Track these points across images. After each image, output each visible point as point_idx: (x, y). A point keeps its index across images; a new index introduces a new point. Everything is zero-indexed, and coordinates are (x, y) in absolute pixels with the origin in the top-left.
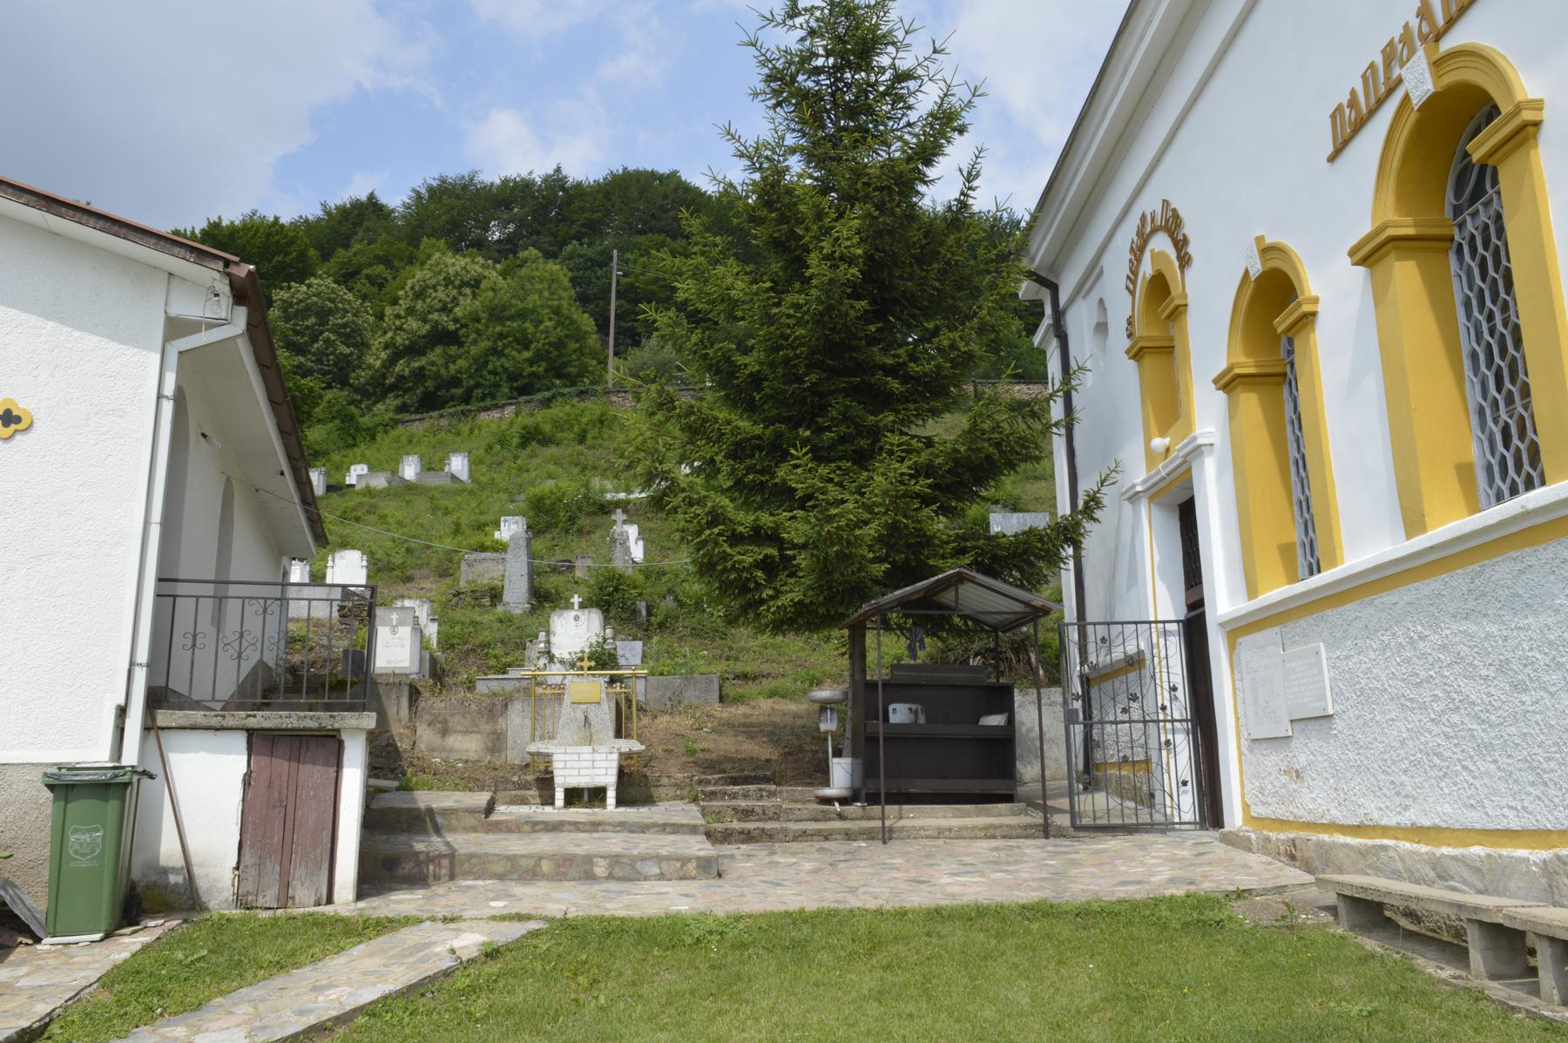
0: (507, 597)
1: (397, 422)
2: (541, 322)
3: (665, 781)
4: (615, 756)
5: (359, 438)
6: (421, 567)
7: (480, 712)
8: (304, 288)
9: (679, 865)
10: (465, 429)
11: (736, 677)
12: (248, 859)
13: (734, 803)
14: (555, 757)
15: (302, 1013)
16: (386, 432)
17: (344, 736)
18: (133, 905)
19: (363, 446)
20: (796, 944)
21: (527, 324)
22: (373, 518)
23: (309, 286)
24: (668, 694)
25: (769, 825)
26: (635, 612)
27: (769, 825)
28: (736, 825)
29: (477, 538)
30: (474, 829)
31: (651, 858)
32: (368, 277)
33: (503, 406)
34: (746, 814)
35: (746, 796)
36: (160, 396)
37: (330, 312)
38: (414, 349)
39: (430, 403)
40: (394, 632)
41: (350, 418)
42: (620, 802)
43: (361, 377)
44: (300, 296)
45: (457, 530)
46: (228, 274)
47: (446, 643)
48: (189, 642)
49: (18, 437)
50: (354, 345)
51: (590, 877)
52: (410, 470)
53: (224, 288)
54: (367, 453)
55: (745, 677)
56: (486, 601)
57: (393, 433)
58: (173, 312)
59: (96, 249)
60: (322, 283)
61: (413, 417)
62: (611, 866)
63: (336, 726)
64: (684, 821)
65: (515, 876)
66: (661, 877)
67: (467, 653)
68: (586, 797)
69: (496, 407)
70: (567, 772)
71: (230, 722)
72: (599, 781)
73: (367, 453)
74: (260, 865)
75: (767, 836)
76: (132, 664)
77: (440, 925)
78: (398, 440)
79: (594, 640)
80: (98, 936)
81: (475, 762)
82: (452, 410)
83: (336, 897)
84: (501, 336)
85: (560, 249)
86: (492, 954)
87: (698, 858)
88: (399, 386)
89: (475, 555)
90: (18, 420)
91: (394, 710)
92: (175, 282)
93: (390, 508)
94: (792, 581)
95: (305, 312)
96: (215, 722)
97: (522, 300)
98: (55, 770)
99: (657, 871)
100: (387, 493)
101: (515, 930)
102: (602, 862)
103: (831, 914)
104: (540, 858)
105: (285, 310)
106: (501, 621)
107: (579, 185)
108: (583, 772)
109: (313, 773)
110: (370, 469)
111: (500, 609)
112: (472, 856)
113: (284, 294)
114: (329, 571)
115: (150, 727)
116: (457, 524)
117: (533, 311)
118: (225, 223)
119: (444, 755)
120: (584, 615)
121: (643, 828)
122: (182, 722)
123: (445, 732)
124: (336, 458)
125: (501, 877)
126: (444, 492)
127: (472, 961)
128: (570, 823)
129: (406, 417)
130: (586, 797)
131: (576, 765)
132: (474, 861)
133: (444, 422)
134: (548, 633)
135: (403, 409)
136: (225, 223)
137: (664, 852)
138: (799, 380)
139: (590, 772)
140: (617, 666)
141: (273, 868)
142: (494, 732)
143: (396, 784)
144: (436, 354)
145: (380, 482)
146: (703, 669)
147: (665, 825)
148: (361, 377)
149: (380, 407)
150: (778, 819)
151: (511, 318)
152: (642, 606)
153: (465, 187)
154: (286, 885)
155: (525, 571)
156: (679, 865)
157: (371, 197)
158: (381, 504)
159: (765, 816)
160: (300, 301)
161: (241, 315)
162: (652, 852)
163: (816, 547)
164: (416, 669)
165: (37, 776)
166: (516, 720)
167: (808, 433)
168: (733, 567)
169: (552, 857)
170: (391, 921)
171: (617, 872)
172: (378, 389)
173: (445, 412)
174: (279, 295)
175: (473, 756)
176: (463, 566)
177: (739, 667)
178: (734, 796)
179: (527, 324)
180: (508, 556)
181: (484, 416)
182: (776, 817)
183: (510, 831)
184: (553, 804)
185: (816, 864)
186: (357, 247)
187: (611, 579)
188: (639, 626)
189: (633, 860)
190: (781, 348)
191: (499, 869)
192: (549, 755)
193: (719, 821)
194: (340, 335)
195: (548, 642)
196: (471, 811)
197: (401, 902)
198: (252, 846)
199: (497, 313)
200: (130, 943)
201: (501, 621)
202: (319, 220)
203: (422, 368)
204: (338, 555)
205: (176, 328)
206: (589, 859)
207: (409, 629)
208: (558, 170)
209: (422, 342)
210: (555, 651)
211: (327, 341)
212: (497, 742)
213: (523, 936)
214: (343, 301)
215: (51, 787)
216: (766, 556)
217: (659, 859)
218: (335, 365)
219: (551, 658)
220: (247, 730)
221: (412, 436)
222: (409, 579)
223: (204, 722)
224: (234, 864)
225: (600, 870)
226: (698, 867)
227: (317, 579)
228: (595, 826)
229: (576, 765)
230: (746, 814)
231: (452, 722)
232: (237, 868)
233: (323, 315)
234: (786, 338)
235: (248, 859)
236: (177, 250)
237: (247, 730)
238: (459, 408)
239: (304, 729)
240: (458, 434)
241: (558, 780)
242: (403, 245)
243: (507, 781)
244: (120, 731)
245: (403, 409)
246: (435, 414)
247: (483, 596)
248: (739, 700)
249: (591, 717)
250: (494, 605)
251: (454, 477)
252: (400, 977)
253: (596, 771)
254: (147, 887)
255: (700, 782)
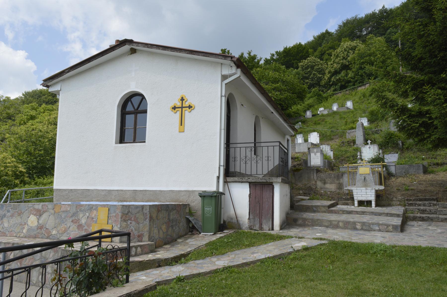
0: (357, 143)
1: (333, 94)
2: (377, 55)
3: (395, 199)
4: (374, 191)
5: (323, 100)
6: (336, 135)
7: (335, 177)
8: (306, 61)
9: (386, 227)
10: (354, 93)
11: (434, 164)
12: (251, 217)
13: (419, 207)
14: (354, 191)
15: (244, 259)
16: (331, 98)
17: (274, 184)
18: (221, 227)
19: (324, 102)
20: (412, 258)
21: (372, 57)
22: (324, 123)
23: (308, 60)
24: (403, 171)
25: (431, 216)
26: (398, 144)
27: (431, 216)
28: (419, 215)
29: (352, 125)
30: (325, 212)
31: (376, 224)
32: (328, 53)
33: (365, 85)
34: (423, 211)
35: (424, 205)
36: (221, 96)
37: (314, 66)
38: (336, 73)
39: (343, 87)
40: (315, 155)
41: (320, 95)
42: (377, 205)
43: (323, 83)
44: (306, 63)
45: (346, 123)
46: (233, 61)
47: (336, 157)
48: (269, 159)
49: (192, 111)
50: (322, 74)
51: (355, 229)
52: (335, 108)
53: (233, 64)
54: (325, 104)
55: (438, 164)
56: (352, 144)
57: (333, 98)
58: (223, 74)
59: (205, 61)
60: (311, 59)
61: (338, 92)
62: (362, 226)
63: (271, 181)
64: (395, 213)
65: (331, 226)
66: (380, 230)
67: (342, 160)
68: (365, 204)
69: (363, 85)
70: (358, 196)
71: (244, 180)
72: (369, 199)
73: (325, 104)
74: (254, 218)
75: (432, 220)
76: (220, 166)
77: (297, 239)
78: (334, 99)
79: (376, 154)
80: (212, 234)
81: (333, 192)
82: (350, 88)
83: (274, 228)
84: (363, 63)
85: (386, 32)
86: (306, 249)
87: (393, 225)
88: (334, 84)
89: (349, 131)
90: (192, 107)
91: (312, 177)
92: (223, 66)
93: (329, 120)
94: (436, 130)
95: (307, 68)
96: (240, 180)
97: (369, 50)
98: (201, 192)
99: (378, 229)
100: (328, 115)
101: (319, 242)
102: (359, 224)
103: (432, 249)
104: (339, 222)
105: (302, 68)
106: (354, 150)
107: (391, 10)
108: (363, 196)
109: (266, 194)
110: (324, 109)
111: (355, 146)
112: (318, 220)
113: (301, 64)
114: (309, 139)
115: (225, 182)
116: (346, 122)
117: (374, 53)
118: (288, 47)
119: (325, 190)
120: (372, 147)
121: (387, 215)
122: (233, 180)
123: (325, 183)
124: (316, 107)
125: (327, 227)
126: (345, 113)
127: (298, 251)
128: (355, 211)
129: (336, 92)
130: (365, 204)
131: (360, 193)
132: (319, 221)
133: (347, 92)
134: (361, 152)
135: (335, 90)
136: (288, 47)
137: (381, 222)
138: (436, 56)
139: (365, 196)
140: (384, 162)
141: (257, 220)
142: (339, 183)
143: (308, 198)
144: (343, 73)
145: (326, 112)
146: (416, 162)
147: (387, 214)
148: (323, 83)
149: (329, 91)
150: (436, 214)
151: (367, 56)
152: (400, 143)
153: (354, 20)
154: (261, 224)
155: (362, 134)
156: (386, 227)
157: (327, 31)
158: (326, 118)
159: (430, 212)
160: (306, 65)
161: (239, 70)
162: (376, 222)
163: (440, 118)
164: (322, 165)
165: (197, 194)
166: (345, 179)
167: (444, 76)
168: (411, 128)
169: (343, 221)
170: (284, 236)
171: (364, 227)
172: (328, 85)
173: (347, 89)
174: (300, 64)
175: (333, 190)
176: (347, 134)
177: (436, 161)
178: (420, 205)
179: (372, 57)
180: (357, 130)
181: (360, 88)
182: (435, 213)
183: (336, 213)
184: (354, 205)
185: (443, 230)
186: (324, 45)
187: (389, 134)
188: (399, 149)
189: (370, 224)
190: (427, 46)
191: (327, 224)
192: (352, 190)
193: (412, 213)
194: (318, 72)
195: (361, 155)
196: (324, 206)
197: (293, 232)
198: (252, 213)
199: (361, 56)
200: (219, 235)
201: (354, 150)
202: (313, 41)
203: (340, 79)
204: (311, 134)
205: (224, 77)
206: (354, 223)
207: (319, 154)
208: (384, 7)
209: (338, 70)
210: (363, 158)
211: (314, 74)
212: (340, 186)
213: (318, 245)
214: (317, 62)
215: (200, 196)
216: (423, 122)
217: (378, 224)
218: (317, 81)
219: (362, 160)
220: (249, 182)
221: (338, 98)
222: (332, 139)
223: (238, 180)
224: (248, 217)
225: (358, 227)
226: (393, 228)
227: (306, 141)
228: (350, 212)
229: (360, 193)
230: (423, 211)
231: (327, 180)
232: (249, 219)
233: (312, 67)
234: (429, 42)
235: (251, 217)
236: (220, 57)
237: (249, 182)
238: (352, 87)
239: (262, 182)
240: (352, 95)
241: (355, 198)
242: (337, 42)
243: (341, 198)
244: (218, 182)
245: (335, 90)
246: (345, 90)
247: (351, 143)
248: (432, 172)
249: (367, 178)
250: (354, 145)
251: (347, 108)
252: (276, 252)
253: (368, 196)
254: (228, 222)
255: (407, 200)
